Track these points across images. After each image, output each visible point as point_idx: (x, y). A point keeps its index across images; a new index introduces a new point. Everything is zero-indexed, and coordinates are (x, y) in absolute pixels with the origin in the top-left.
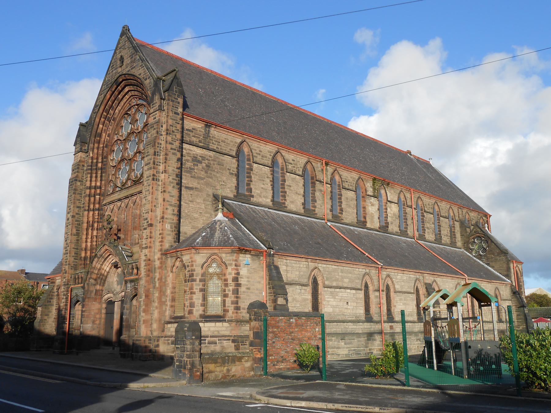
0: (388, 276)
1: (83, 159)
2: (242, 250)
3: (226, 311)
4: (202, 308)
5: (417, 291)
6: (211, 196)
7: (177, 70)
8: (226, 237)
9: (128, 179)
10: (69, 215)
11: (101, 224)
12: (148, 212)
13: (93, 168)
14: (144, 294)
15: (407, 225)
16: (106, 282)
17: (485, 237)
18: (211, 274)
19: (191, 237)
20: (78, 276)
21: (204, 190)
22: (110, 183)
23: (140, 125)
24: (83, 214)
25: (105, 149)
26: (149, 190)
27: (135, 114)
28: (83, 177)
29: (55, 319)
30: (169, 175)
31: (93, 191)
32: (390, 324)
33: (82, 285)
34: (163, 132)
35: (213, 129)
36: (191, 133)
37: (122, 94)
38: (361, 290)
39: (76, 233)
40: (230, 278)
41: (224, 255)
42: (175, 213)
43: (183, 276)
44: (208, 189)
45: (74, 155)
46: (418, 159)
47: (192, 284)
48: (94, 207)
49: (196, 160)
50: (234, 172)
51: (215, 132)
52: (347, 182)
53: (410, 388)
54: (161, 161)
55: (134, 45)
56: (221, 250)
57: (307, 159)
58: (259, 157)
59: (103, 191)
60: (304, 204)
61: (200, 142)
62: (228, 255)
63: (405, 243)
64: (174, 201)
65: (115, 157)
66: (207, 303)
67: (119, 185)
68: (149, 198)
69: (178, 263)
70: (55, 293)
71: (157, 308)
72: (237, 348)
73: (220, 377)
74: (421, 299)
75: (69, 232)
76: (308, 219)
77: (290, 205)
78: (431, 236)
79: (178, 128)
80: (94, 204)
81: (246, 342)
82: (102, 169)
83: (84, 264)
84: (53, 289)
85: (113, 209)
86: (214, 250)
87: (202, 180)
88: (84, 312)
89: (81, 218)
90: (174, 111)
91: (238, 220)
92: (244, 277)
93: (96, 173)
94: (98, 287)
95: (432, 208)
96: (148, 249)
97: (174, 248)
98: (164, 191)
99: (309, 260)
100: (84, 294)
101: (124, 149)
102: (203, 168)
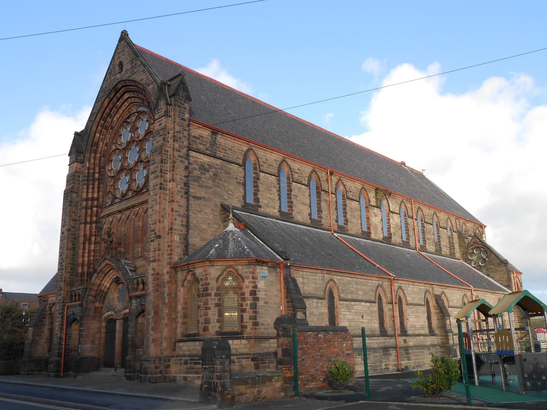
0: (400, 288)
1: (78, 170)
2: (260, 262)
3: (243, 327)
4: (218, 325)
5: (428, 303)
6: (219, 206)
7: (183, 74)
8: (240, 249)
9: (129, 189)
10: (64, 229)
11: (98, 237)
12: (156, 223)
13: (89, 179)
14: (153, 311)
15: (409, 236)
16: (106, 299)
17: (484, 247)
18: (227, 288)
19: (203, 249)
20: (75, 293)
21: (212, 200)
22: (108, 194)
23: (141, 132)
24: (79, 227)
25: (102, 158)
26: (156, 200)
27: (135, 121)
28: (79, 188)
29: (47, 339)
30: (177, 184)
31: (90, 203)
32: (404, 338)
33: (80, 302)
34: (169, 139)
35: (219, 136)
36: (197, 140)
37: (121, 101)
38: (374, 302)
39: (72, 247)
40: (247, 291)
41: (240, 268)
42: (184, 223)
43: (196, 291)
44: (215, 199)
45: (69, 165)
46: (412, 170)
47: (207, 299)
48: (91, 219)
49: (203, 168)
50: (241, 182)
51: (222, 140)
52: (351, 192)
53: (473, 407)
54: (168, 169)
55: (135, 49)
56: (237, 262)
57: (312, 168)
58: (266, 166)
59: (101, 203)
60: (310, 215)
61: (207, 149)
62: (245, 267)
63: (408, 254)
64: (182, 211)
65: (115, 166)
66: (223, 319)
67: (118, 196)
68: (157, 208)
69: (189, 277)
70: (47, 312)
71: (166, 325)
72: (257, 367)
73: (251, 399)
74: (431, 311)
75: (64, 247)
76: (315, 230)
77: (296, 216)
78: (432, 247)
79: (185, 135)
80: (91, 216)
81: (265, 360)
82: (99, 179)
83: (81, 281)
84: (45, 308)
85: (138, 212)
86: (230, 262)
87: (210, 189)
88: (82, 332)
89: (77, 231)
90: (181, 117)
91: (250, 230)
92: (262, 291)
93: (93, 184)
94: (98, 304)
95: (431, 219)
96: (157, 263)
97: (185, 261)
98: (173, 201)
99: (325, 272)
100: (82, 312)
101: (124, 158)
102: (210, 177)
